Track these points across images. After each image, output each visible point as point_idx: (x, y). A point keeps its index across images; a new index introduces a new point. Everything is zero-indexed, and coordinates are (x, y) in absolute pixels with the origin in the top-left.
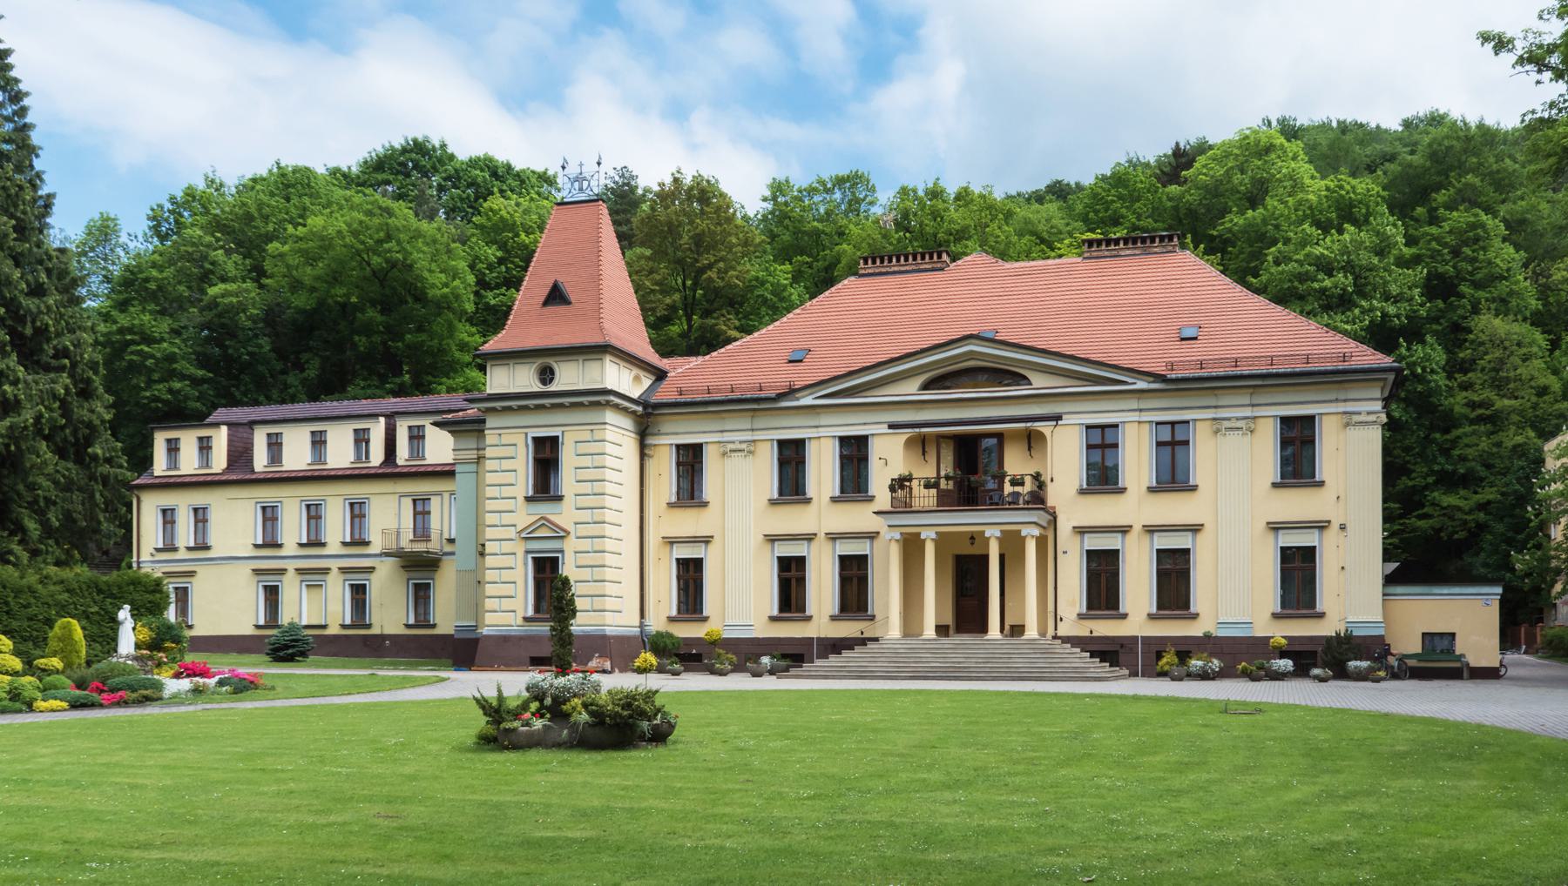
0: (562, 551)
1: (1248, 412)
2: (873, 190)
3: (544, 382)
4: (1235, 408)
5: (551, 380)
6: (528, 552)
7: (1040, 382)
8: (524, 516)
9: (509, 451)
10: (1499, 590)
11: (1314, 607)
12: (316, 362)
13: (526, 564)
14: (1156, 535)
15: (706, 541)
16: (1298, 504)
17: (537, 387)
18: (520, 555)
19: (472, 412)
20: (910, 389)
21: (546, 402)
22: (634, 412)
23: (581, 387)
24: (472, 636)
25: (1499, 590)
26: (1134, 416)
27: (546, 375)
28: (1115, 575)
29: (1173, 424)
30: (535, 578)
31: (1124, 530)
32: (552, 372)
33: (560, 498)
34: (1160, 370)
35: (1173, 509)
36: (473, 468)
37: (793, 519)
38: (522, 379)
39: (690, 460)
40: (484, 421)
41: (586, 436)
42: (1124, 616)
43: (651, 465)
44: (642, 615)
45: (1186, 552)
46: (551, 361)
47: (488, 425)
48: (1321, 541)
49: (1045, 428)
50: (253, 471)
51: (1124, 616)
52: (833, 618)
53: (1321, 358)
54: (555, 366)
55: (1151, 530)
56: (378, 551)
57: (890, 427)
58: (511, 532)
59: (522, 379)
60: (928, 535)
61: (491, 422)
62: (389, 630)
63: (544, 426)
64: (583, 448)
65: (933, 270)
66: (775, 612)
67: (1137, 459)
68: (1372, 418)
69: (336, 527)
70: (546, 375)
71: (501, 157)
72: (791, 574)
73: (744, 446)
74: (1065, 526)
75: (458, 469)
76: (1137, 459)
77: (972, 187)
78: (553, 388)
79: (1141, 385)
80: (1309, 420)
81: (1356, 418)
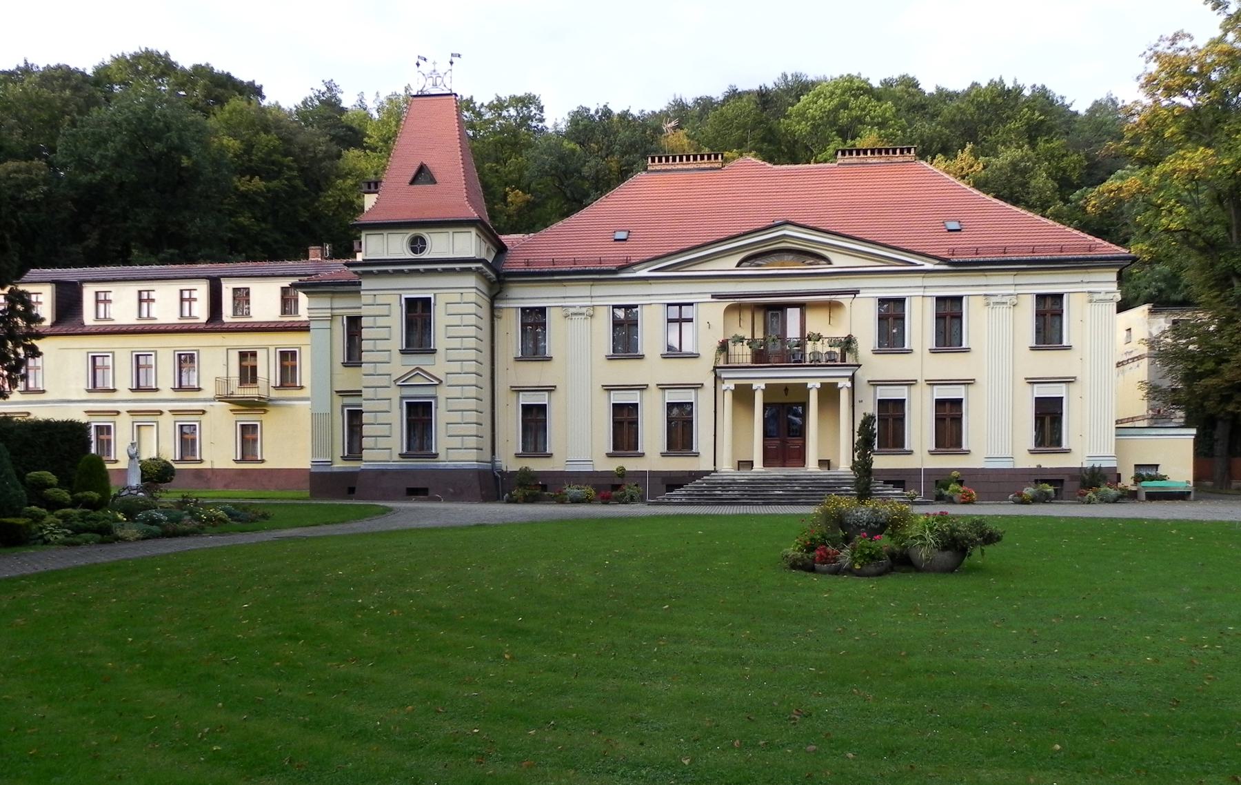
0: (435, 397)
1: (1011, 290)
2: (541, 109)
3: (414, 250)
4: (1002, 284)
5: (422, 250)
6: (402, 398)
7: (840, 262)
8: (400, 366)
9: (384, 310)
10: (1194, 431)
11: (903, 446)
12: (95, 235)
13: (401, 408)
14: (935, 387)
15: (550, 389)
16: (1050, 363)
17: (410, 255)
18: (396, 401)
19: (348, 274)
20: (728, 265)
21: (421, 267)
22: (489, 280)
23: (451, 256)
24: (328, 470)
25: (1194, 431)
26: (920, 292)
27: (417, 244)
28: (900, 420)
29: (680, 305)
30: (408, 420)
31: (642, 388)
32: (423, 241)
33: (434, 351)
34: (945, 255)
35: (950, 365)
36: (327, 324)
37: (626, 372)
38: (395, 246)
39: (534, 320)
40: (360, 284)
41: (457, 298)
42: (642, 455)
43: (500, 326)
44: (493, 452)
45: (958, 402)
46: (423, 232)
47: (363, 287)
48: (909, 392)
49: (845, 300)
50: (82, 324)
51: (642, 455)
52: (932, 453)
53: (992, 249)
54: (426, 236)
55: (663, 387)
56: (212, 396)
57: (713, 297)
58: (384, 381)
59: (395, 246)
60: (759, 385)
61: (366, 284)
62: (218, 465)
63: (417, 288)
64: (452, 309)
65: (711, 169)
66: (1033, 447)
67: (920, 323)
68: (1110, 296)
69: (165, 373)
70: (417, 244)
71: (219, 67)
72: (625, 422)
73: (584, 310)
74: (863, 375)
75: (312, 325)
76: (920, 323)
77: (631, 111)
78: (425, 255)
79: (929, 266)
80: (1059, 297)
81: (1096, 297)
